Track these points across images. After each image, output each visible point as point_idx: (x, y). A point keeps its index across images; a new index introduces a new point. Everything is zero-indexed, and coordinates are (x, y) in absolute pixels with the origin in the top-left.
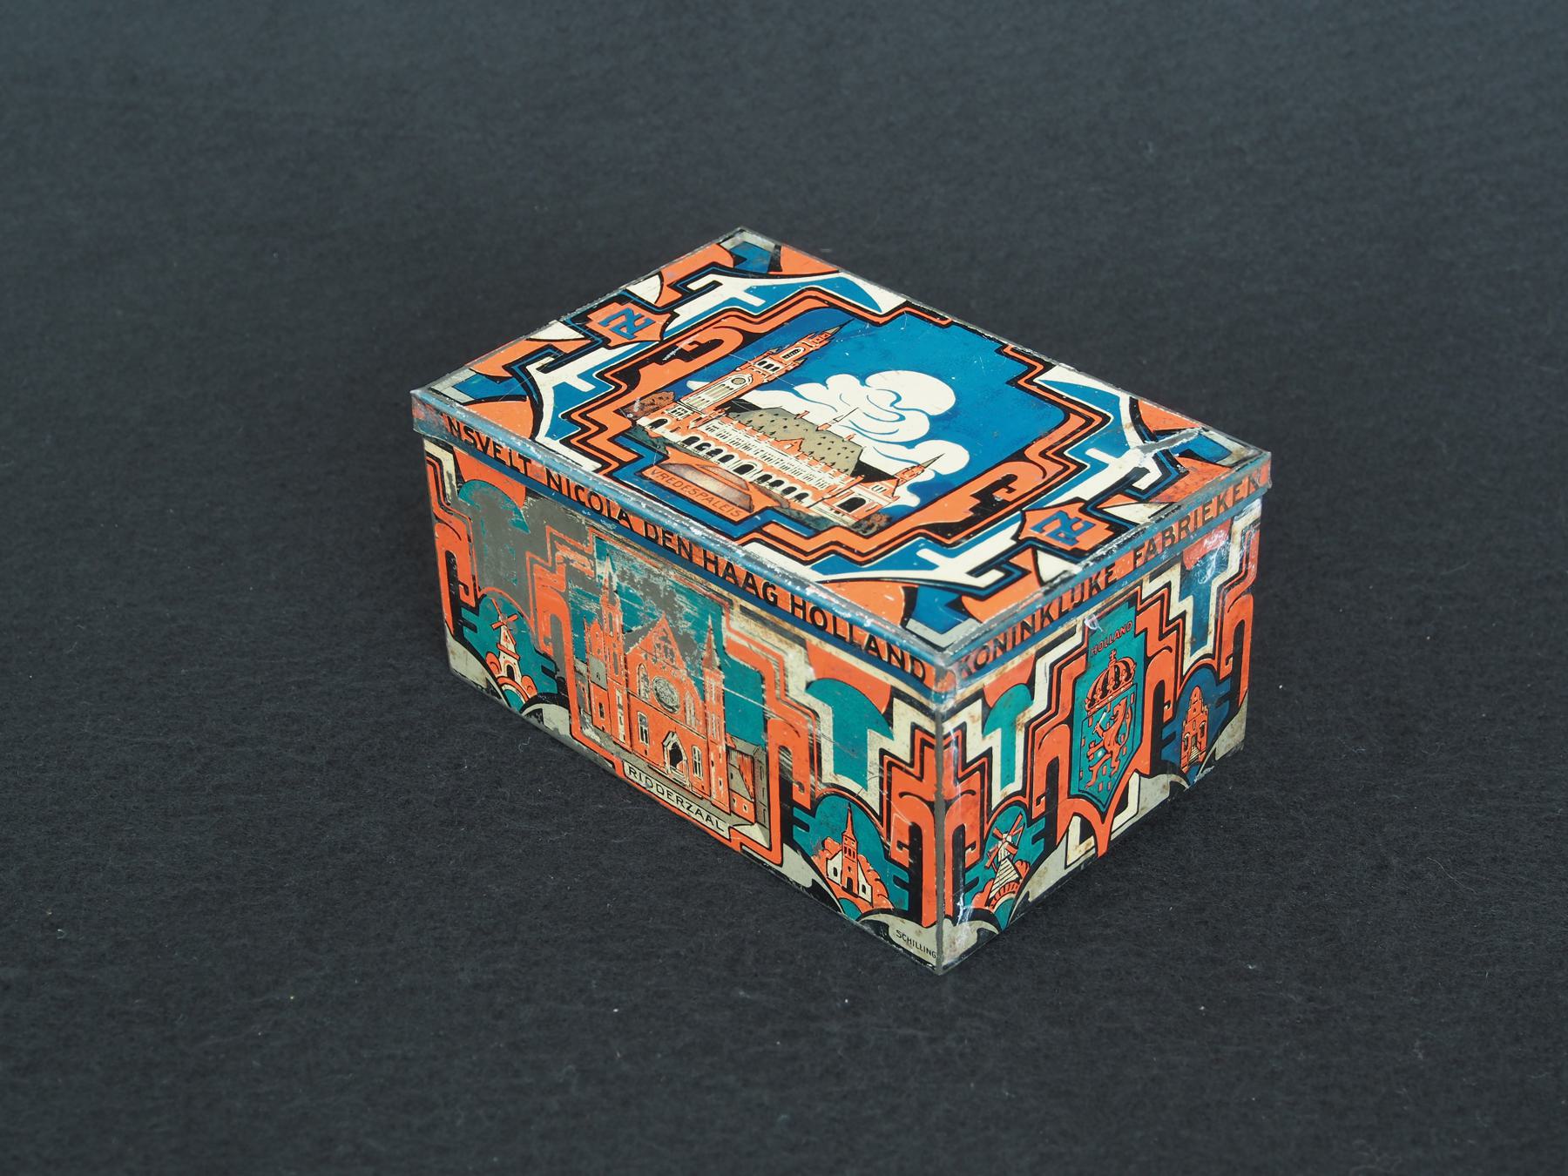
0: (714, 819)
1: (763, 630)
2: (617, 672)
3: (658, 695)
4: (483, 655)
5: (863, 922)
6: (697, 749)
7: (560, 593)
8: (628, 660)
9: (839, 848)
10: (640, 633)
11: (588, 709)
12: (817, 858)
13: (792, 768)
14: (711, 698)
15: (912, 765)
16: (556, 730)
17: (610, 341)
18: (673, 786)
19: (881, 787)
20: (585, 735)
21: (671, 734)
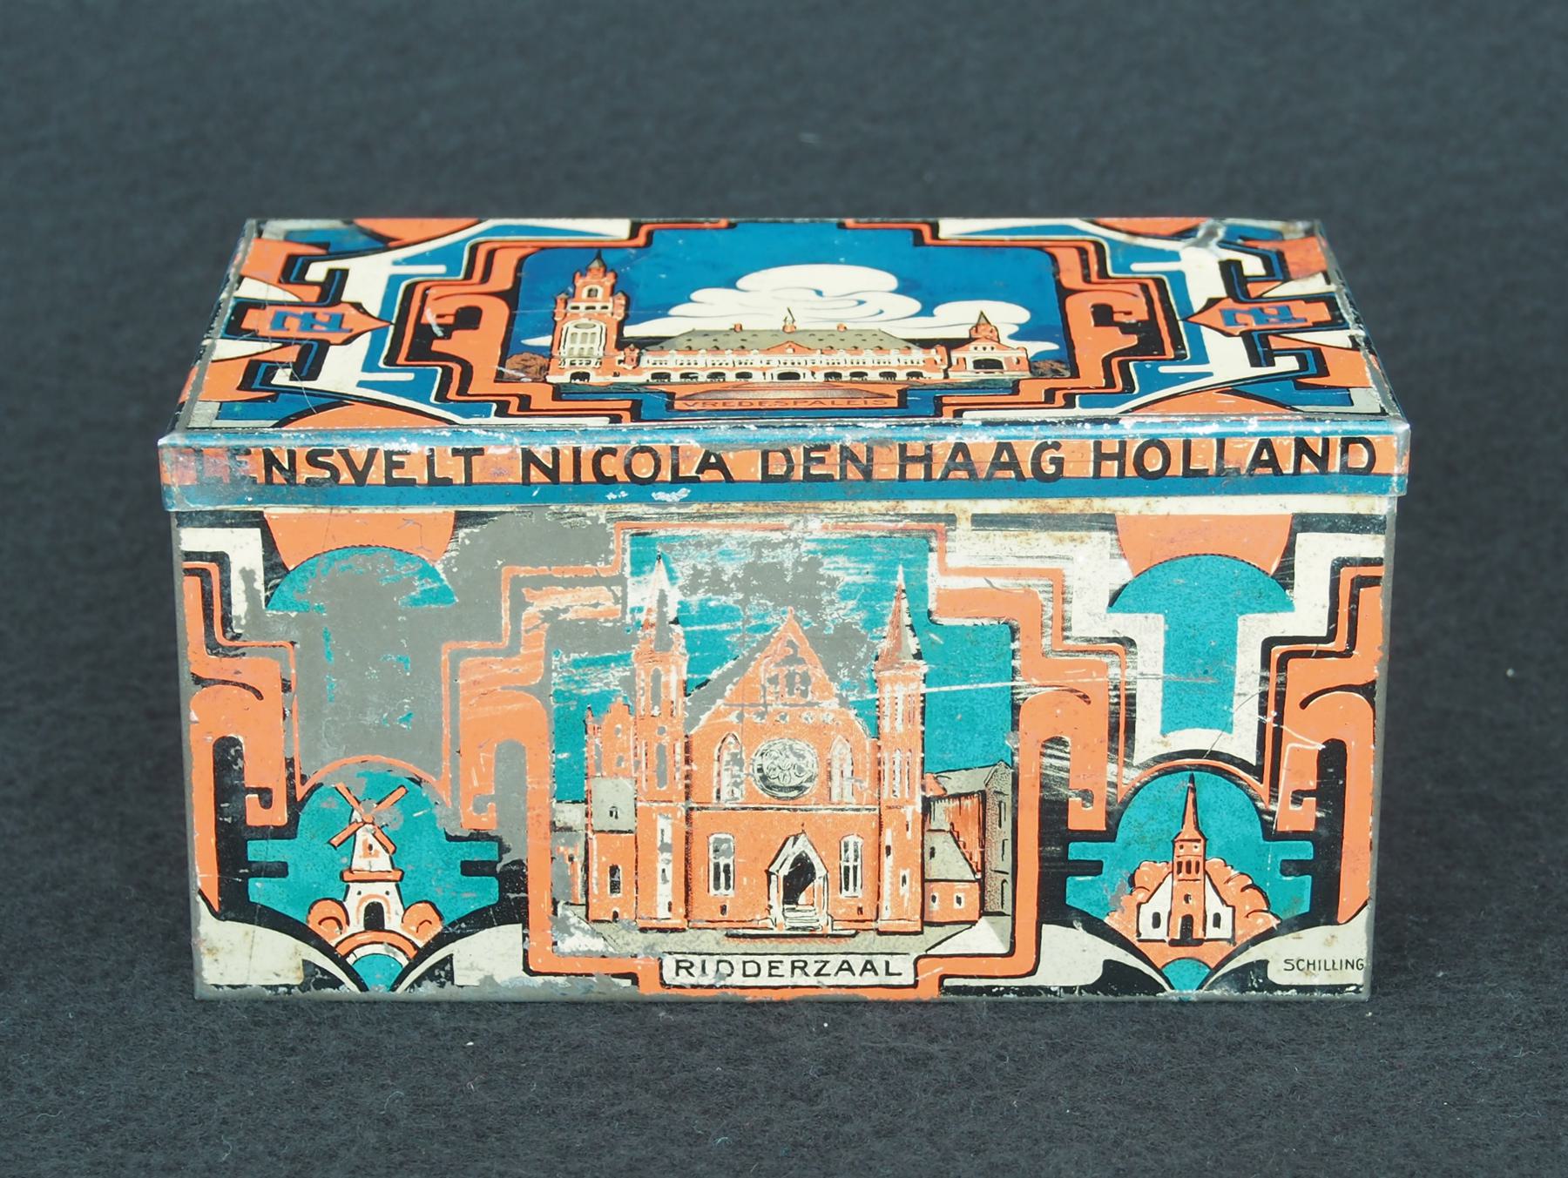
0: (879, 962)
1: (1023, 538)
2: (662, 780)
3: (764, 778)
4: (299, 916)
5: (1212, 987)
6: (851, 840)
7: (528, 689)
8: (695, 744)
9: (1166, 870)
10: (726, 678)
11: (579, 888)
12: (1116, 915)
13: (1068, 771)
14: (896, 724)
15: (1332, 635)
16: (489, 980)
17: (674, 394)
18: (794, 945)
19: (1263, 711)
20: (564, 955)
21: (791, 840)
